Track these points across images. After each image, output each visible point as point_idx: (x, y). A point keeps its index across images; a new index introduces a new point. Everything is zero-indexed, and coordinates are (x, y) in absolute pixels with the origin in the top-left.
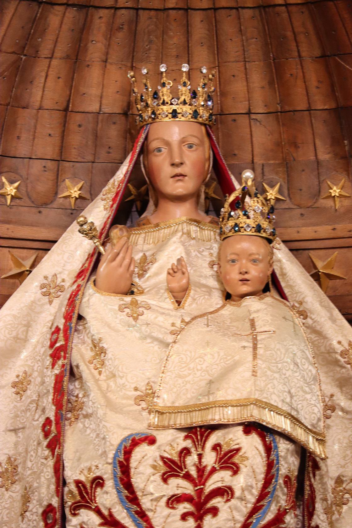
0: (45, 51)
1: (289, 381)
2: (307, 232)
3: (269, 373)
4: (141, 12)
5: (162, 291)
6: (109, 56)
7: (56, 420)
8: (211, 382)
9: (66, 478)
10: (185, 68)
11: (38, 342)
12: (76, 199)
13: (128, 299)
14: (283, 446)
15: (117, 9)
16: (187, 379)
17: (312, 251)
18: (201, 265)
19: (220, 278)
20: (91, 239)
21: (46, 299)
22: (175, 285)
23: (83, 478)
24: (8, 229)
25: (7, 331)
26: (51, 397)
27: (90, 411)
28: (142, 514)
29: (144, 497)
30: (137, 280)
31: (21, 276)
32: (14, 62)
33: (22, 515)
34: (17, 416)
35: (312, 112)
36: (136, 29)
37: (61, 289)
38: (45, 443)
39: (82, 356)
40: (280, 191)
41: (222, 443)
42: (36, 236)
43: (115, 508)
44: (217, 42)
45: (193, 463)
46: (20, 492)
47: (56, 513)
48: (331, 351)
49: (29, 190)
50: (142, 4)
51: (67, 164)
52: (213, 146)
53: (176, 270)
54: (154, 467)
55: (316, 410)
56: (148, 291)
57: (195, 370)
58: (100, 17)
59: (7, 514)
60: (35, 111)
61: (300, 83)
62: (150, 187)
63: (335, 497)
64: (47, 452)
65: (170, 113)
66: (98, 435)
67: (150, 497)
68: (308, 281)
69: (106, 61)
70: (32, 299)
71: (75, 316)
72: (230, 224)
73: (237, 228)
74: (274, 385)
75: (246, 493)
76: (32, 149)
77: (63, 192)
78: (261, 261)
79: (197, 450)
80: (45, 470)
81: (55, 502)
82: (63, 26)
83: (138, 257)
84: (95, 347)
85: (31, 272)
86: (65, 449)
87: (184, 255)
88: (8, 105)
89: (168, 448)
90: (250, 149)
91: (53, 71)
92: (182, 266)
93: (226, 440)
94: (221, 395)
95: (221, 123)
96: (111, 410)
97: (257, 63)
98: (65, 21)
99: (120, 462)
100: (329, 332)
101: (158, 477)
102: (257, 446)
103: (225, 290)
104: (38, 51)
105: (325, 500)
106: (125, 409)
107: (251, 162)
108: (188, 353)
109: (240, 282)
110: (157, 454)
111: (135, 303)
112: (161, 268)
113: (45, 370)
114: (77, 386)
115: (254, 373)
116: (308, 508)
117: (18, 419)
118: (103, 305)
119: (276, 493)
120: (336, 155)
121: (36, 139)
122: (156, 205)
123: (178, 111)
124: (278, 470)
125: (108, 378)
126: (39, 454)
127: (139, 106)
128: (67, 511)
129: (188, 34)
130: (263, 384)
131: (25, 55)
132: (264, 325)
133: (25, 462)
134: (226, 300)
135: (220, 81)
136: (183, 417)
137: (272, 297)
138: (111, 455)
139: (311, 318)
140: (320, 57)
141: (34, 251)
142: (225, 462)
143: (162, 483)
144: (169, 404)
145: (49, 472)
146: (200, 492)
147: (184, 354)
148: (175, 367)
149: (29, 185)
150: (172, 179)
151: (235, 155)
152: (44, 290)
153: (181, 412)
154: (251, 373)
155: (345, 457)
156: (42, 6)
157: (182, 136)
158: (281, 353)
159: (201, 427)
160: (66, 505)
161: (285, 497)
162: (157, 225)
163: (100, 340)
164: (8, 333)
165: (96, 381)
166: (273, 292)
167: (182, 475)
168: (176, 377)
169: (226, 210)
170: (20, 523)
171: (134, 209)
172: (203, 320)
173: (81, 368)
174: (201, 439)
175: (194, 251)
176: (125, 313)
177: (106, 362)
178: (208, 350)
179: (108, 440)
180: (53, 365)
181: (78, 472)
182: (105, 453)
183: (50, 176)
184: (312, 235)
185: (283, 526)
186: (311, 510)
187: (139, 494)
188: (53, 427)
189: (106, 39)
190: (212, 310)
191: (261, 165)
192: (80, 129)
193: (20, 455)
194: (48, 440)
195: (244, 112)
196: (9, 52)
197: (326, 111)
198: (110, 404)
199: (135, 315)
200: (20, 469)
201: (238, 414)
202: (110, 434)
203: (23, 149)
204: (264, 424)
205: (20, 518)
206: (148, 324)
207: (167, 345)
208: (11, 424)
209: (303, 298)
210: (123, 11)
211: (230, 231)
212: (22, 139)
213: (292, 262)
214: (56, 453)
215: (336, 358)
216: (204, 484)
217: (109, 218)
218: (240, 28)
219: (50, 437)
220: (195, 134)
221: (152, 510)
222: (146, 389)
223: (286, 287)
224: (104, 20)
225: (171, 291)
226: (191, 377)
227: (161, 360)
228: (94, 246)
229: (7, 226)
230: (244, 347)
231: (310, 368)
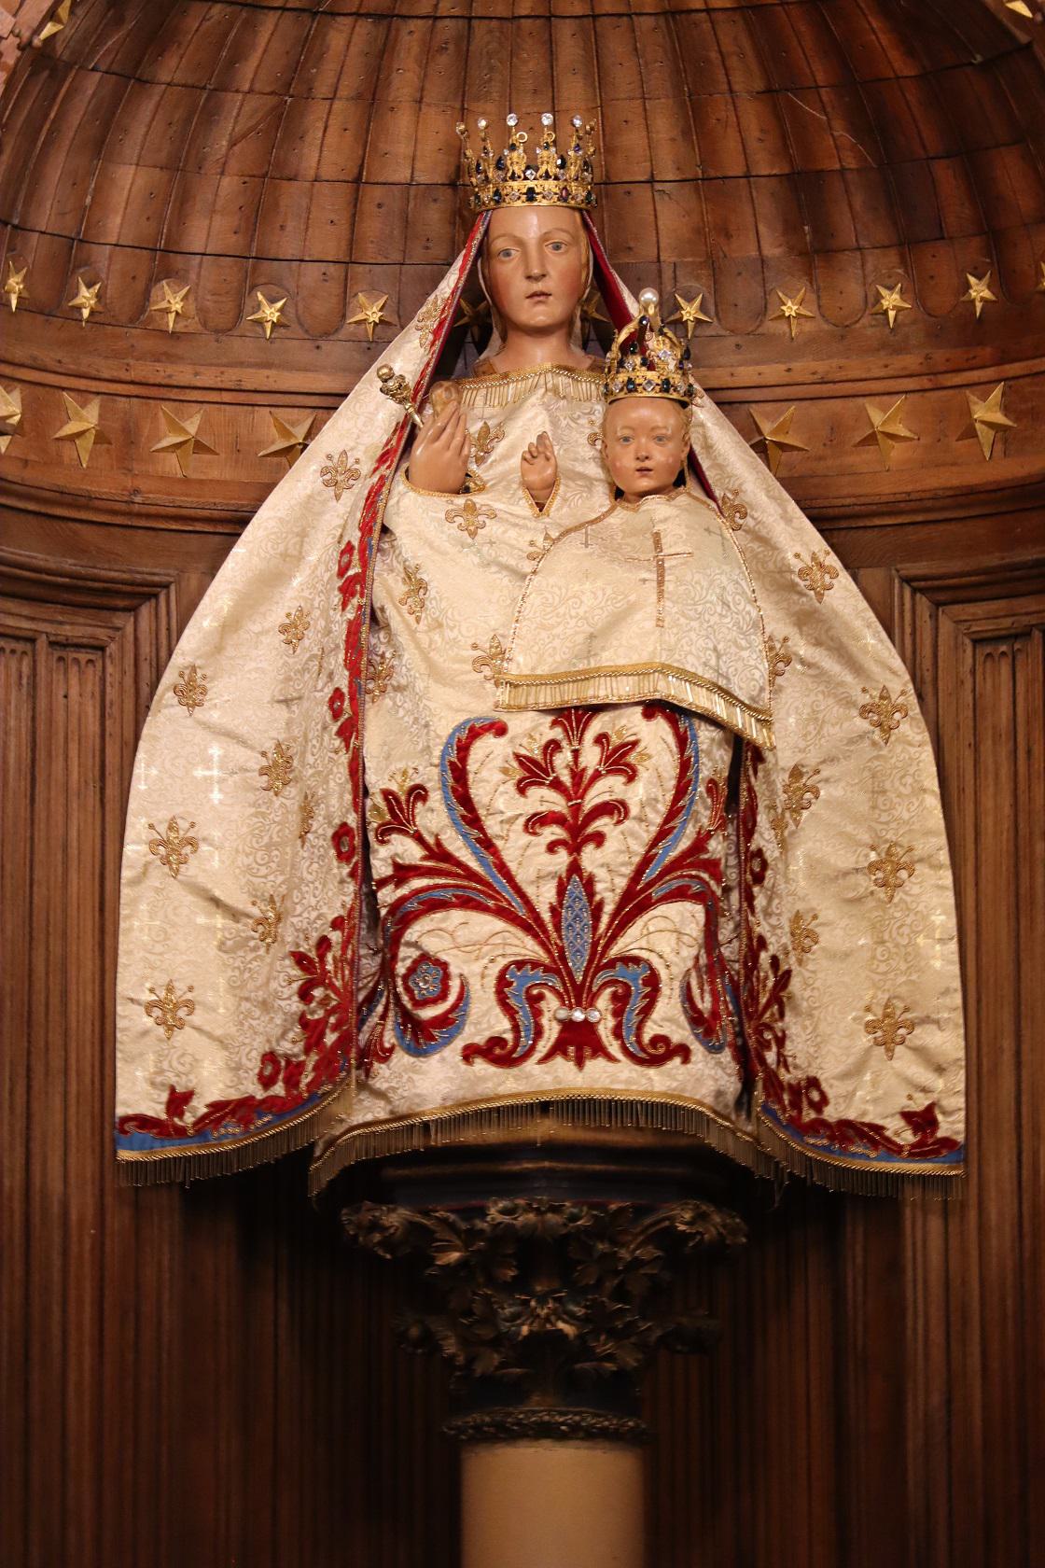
0: (322, 89)
2: (747, 374)
3: (683, 620)
4: (475, 23)
5: (515, 486)
6: (425, 93)
7: (350, 693)
8: (592, 636)
9: (369, 786)
10: (547, 119)
11: (319, 560)
12: (376, 324)
13: (460, 501)
14: (705, 734)
15: (436, 18)
16: (554, 632)
17: (754, 405)
18: (576, 441)
19: (606, 462)
20: (400, 402)
21: (331, 491)
22: (534, 478)
23: (394, 787)
24: (268, 377)
25: (270, 544)
26: (342, 656)
27: (403, 682)
28: (487, 844)
29: (490, 817)
30: (473, 467)
31: (291, 453)
32: (274, 109)
33: (301, 837)
34: (288, 679)
35: (752, 179)
36: (468, 50)
37: (354, 475)
38: (335, 728)
39: (389, 592)
40: (703, 308)
41: (610, 733)
42: (314, 386)
43: (446, 833)
44: (598, 68)
45: (564, 765)
46: (297, 798)
47: (353, 837)
48: (784, 569)
49: (300, 312)
50: (478, 10)
51: (360, 268)
52: (593, 243)
53: (535, 454)
54: (505, 771)
55: (757, 674)
56: (493, 485)
57: (567, 616)
59: (278, 832)
60: (307, 184)
61: (732, 133)
62: (493, 311)
63: (790, 798)
64: (338, 742)
66: (416, 720)
67: (500, 818)
68: (747, 458)
69: (420, 101)
70: (308, 492)
71: (377, 528)
72: (621, 380)
73: (631, 386)
74: (691, 640)
75: (647, 810)
76: (305, 246)
77: (354, 315)
78: (669, 438)
79: (571, 744)
80: (335, 770)
81: (352, 820)
83: (475, 428)
84: (409, 578)
85: (305, 446)
86: (366, 740)
87: (548, 428)
88: (264, 176)
89: (525, 741)
90: (655, 239)
92: (545, 447)
93: (617, 728)
94: (608, 658)
95: (607, 196)
96: (436, 681)
97: (663, 100)
98: (354, 40)
99: (452, 763)
100: (781, 539)
101: (510, 787)
103: (614, 484)
104: (311, 89)
105: (772, 807)
106: (457, 679)
107: (655, 260)
108: (556, 589)
110: (510, 751)
111: (471, 509)
112: (513, 448)
113: (332, 612)
114: (382, 640)
115: (660, 622)
116: (745, 824)
117: (291, 683)
118: (421, 511)
119: (694, 808)
120: (791, 249)
121: (310, 230)
122: (504, 338)
123: (537, 191)
124: (697, 772)
125: (430, 629)
126: (325, 744)
127: (474, 180)
128: (371, 836)
130: (673, 640)
132: (675, 543)
133: (303, 753)
134: (616, 499)
135: (603, 130)
136: (549, 691)
137: (689, 494)
138: (437, 752)
139: (752, 517)
140: (763, 92)
141: (309, 411)
142: (615, 763)
143: (517, 796)
144: (526, 672)
145: (341, 773)
146: (576, 809)
147: (549, 592)
148: (535, 613)
149: (301, 306)
150: (528, 300)
151: (630, 248)
152: (326, 477)
153: (546, 684)
154: (654, 623)
155: (805, 735)
156: (318, 18)
157: (544, 231)
159: (577, 708)
160: (369, 827)
161: (708, 813)
162: (505, 376)
163: (417, 568)
164: (272, 547)
165: (413, 633)
166: (691, 484)
168: (537, 628)
169: (613, 356)
170: (299, 849)
171: (469, 339)
172: (577, 537)
173: (388, 612)
174: (578, 728)
175: (565, 418)
176: (455, 525)
177: (427, 603)
178: (587, 586)
179: (432, 728)
180: (344, 605)
181: (387, 777)
182: (427, 749)
183: (334, 288)
184: (756, 380)
185: (706, 856)
186: (750, 825)
187: (482, 812)
188: (347, 703)
189: (420, 67)
190: (594, 516)
193: (295, 741)
194: (339, 723)
195: (642, 179)
198: (434, 672)
199: (472, 528)
200: (295, 763)
201: (634, 687)
202: (435, 719)
203: (288, 245)
204: (675, 702)
205: (299, 842)
206: (492, 543)
207: (524, 577)
208: (281, 690)
209: (741, 485)
210: (447, 22)
211: (621, 390)
213: (722, 427)
214: (351, 746)
215: (792, 581)
216: (582, 797)
217: (428, 364)
218: (635, 45)
219: (342, 720)
220: (564, 227)
221: (502, 838)
222: (491, 647)
223: (711, 467)
225: (529, 487)
226: (561, 628)
227: (514, 600)
228: (404, 413)
229: (266, 372)
230: (644, 581)
231: (749, 608)
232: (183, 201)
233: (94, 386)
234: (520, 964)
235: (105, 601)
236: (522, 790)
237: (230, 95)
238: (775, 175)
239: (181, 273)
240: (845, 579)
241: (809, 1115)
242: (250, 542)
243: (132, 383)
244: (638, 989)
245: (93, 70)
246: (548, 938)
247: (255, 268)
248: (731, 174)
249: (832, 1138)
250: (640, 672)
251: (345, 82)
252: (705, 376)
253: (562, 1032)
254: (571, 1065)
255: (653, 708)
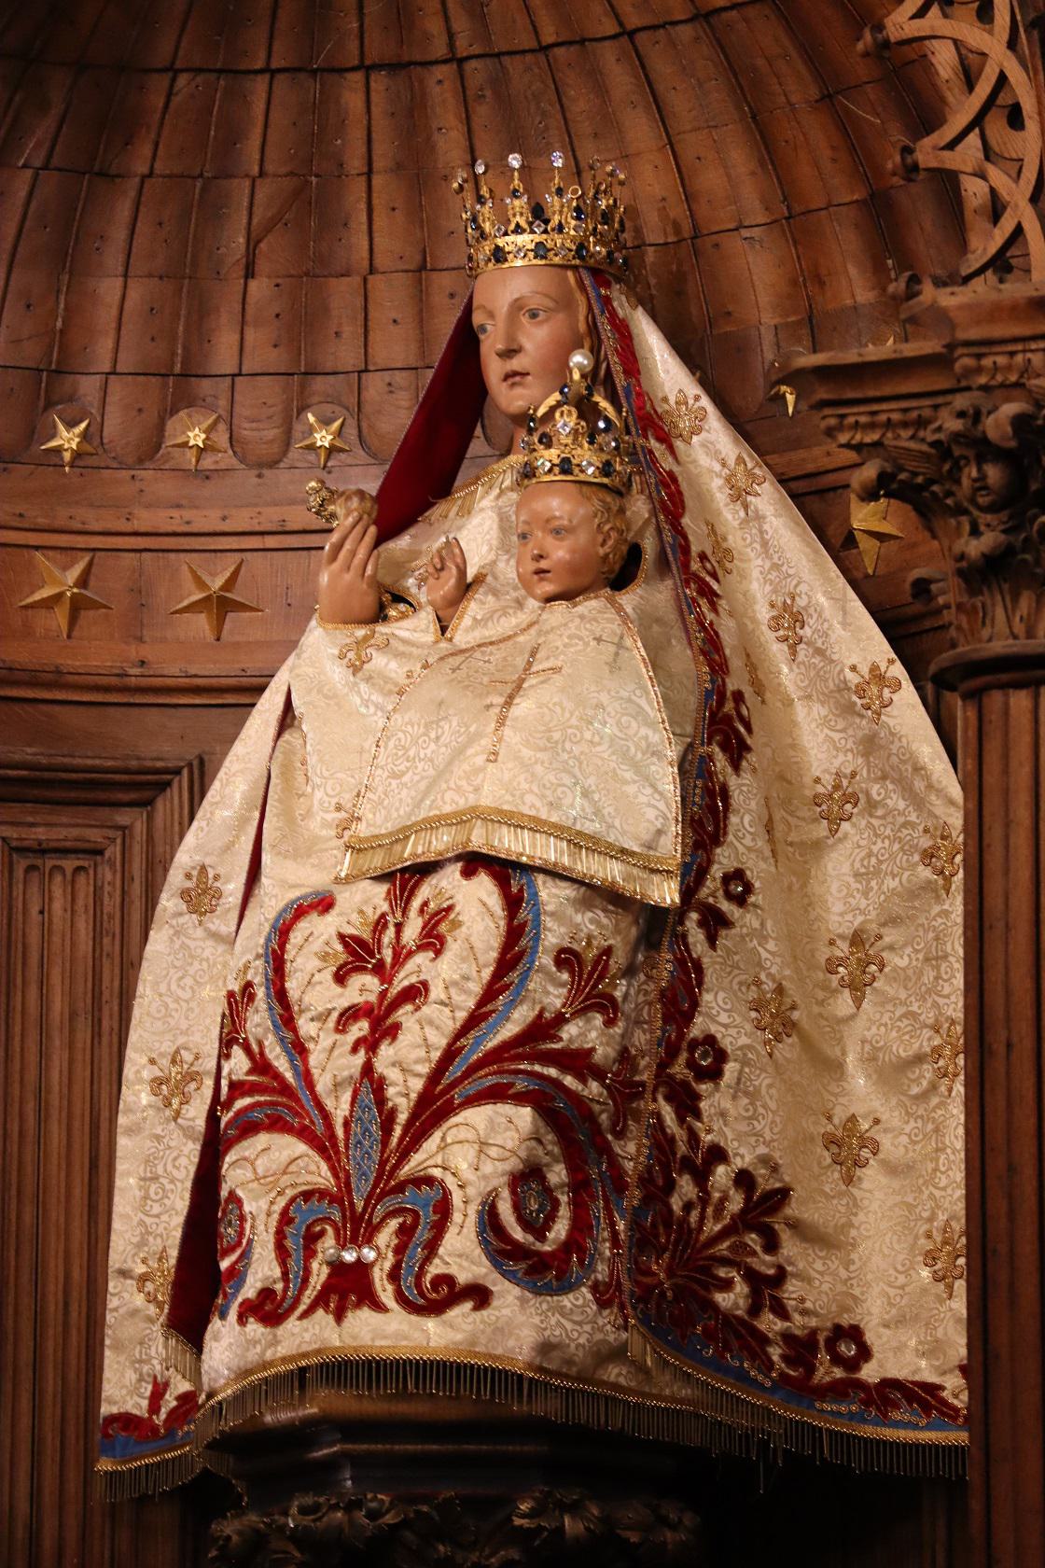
0: (355, 163)
1: (581, 763)
10: (515, 161)
14: (550, 894)
54: (324, 957)
58: (440, 82)
82: (374, 109)
99: (274, 951)
101: (327, 975)
102: (485, 898)
109: (536, 577)
110: (332, 931)
123: (507, 249)
124: (537, 938)
129: (600, 88)
151: (275, 346)
224: (446, 84)
232: (201, 316)
233: (81, 541)
234: (307, 1195)
235: (102, 796)
236: (340, 978)
237: (236, 182)
238: (857, 201)
239: (209, 400)
240: (908, 693)
241: (827, 1372)
243: (136, 534)
244: (428, 1217)
245: (24, 166)
246: (339, 1162)
247: (303, 387)
249: (867, 1403)
250: (461, 819)
253: (330, 1276)
254: (331, 1318)
255: (473, 862)
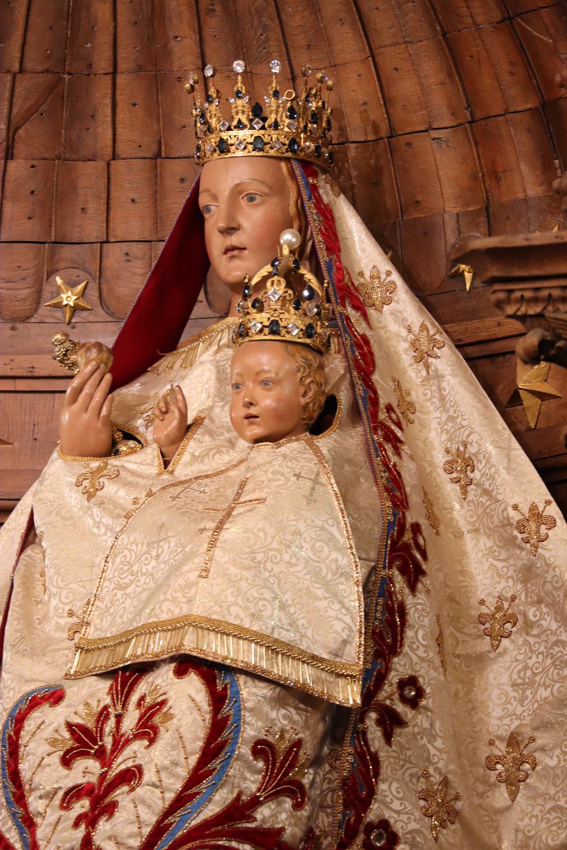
0: (102, 63)
10: (239, 66)
54: (53, 742)
65: (251, 143)
91: (122, 94)
99: (10, 737)
102: (194, 695)
104: (91, 65)
109: (246, 421)
110: (61, 721)
123: (230, 142)
124: (237, 730)
131: (69, 74)
140: (502, 21)
151: (418, 202)
158: (266, 534)
167: (93, 751)
168: (115, 588)
191: (455, 216)
192: (184, 185)
196: (39, 71)
197: (524, 113)
212: (90, 212)
236: (67, 761)
238: (530, 109)
242: (11, 530)
247: (52, 254)
248: (493, 114)
250: (175, 626)
251: (122, 54)
252: (477, 328)
